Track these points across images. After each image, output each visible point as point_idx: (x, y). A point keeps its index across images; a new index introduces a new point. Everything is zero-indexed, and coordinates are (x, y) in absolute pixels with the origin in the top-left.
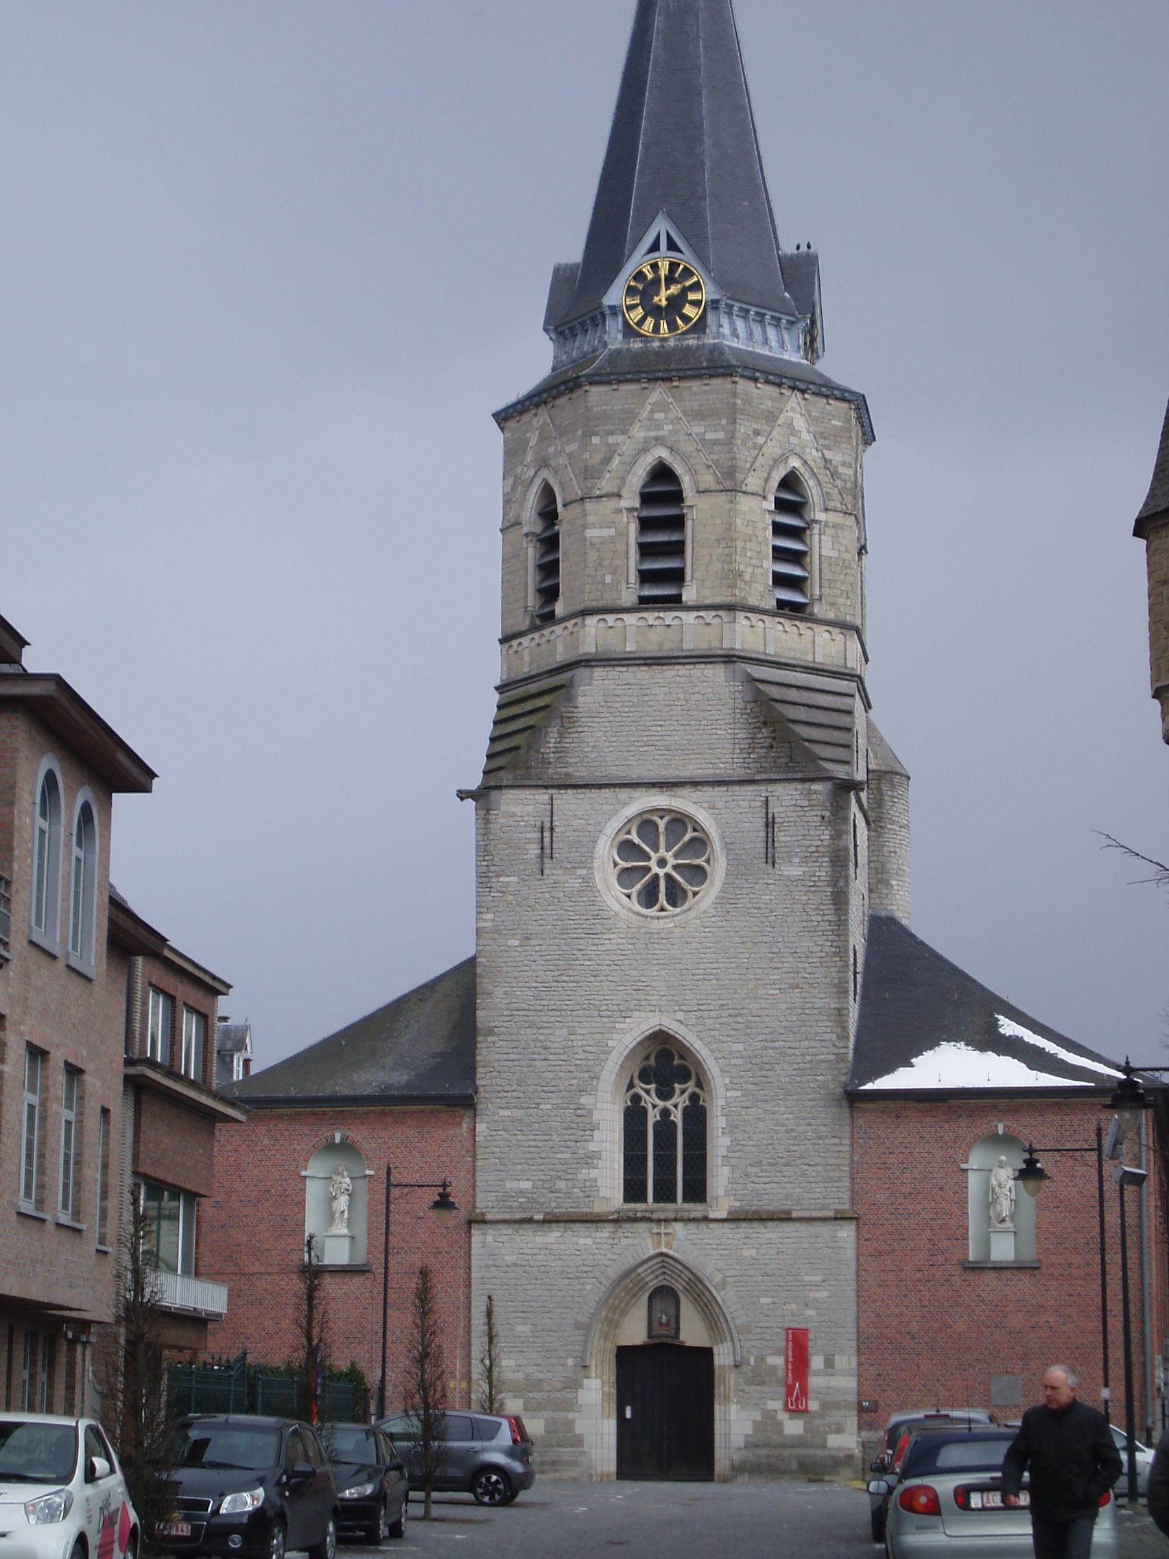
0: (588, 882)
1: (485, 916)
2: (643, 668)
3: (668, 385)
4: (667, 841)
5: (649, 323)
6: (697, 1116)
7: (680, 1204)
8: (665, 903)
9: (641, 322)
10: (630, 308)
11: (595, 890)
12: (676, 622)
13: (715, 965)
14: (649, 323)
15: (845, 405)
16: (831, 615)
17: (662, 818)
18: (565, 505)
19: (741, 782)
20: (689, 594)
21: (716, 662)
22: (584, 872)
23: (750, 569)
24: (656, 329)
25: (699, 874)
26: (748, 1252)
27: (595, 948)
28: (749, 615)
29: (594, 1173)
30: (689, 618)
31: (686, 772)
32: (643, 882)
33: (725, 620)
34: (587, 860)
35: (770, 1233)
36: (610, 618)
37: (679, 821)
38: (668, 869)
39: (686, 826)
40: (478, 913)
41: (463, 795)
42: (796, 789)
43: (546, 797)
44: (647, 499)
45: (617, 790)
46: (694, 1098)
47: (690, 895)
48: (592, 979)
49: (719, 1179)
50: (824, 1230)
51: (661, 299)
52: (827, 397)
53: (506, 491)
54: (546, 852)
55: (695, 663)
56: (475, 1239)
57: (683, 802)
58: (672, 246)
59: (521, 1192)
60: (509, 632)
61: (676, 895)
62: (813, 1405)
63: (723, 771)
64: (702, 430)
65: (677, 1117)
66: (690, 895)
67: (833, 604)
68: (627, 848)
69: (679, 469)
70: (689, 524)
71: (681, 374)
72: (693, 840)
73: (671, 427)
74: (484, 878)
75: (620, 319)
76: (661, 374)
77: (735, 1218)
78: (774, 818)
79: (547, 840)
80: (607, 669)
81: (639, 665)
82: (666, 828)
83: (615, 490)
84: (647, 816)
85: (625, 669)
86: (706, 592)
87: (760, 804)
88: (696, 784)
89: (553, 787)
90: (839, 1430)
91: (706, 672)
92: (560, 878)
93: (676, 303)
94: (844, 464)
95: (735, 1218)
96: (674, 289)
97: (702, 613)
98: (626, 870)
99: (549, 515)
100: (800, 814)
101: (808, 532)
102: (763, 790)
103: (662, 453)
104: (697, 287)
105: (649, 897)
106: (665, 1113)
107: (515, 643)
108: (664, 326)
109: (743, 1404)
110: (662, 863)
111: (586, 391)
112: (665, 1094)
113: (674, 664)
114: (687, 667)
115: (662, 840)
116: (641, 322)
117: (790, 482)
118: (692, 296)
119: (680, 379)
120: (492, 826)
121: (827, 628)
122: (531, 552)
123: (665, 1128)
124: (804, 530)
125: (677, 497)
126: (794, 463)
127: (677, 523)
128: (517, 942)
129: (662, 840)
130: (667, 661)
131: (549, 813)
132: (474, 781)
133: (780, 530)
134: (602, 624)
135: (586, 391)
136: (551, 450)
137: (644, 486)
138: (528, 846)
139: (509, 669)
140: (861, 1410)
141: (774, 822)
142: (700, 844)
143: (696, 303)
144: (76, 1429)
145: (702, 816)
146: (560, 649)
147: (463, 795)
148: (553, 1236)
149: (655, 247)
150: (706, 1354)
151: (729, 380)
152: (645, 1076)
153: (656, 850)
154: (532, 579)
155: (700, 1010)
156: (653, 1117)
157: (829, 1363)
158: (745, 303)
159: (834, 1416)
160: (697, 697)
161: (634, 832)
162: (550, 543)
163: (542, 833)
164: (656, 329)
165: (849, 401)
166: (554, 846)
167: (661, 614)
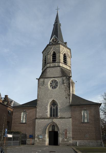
0: (47, 87)
6: (57, 108)
7: (55, 117)
20: (56, 62)
25: (57, 86)
26: (61, 121)
29: (47, 114)
30: (56, 63)
31: (55, 76)
35: (64, 119)
36: (50, 64)
37: (55, 81)
41: (37, 79)
46: (57, 107)
49: (59, 114)
50: (69, 119)
53: (59, 131)
54: (44, 84)
56: (36, 120)
57: (56, 79)
58: (55, 37)
59: (40, 116)
61: (55, 88)
62: (68, 137)
63: (59, 76)
65: (55, 108)
68: (51, 83)
74: (38, 87)
77: (60, 118)
88: (57, 77)
90: (70, 140)
93: (56, 41)
95: (60, 118)
102: (63, 78)
103: (54, 50)
105: (53, 88)
106: (54, 108)
109: (61, 137)
110: (54, 85)
112: (54, 106)
123: (54, 109)
126: (65, 52)
127: (55, 56)
140: (72, 138)
142: (57, 83)
144: (77, 142)
145: (57, 80)
147: (37, 79)
148: (43, 120)
150: (57, 132)
152: (52, 105)
156: (53, 109)
157: (69, 133)
159: (70, 139)
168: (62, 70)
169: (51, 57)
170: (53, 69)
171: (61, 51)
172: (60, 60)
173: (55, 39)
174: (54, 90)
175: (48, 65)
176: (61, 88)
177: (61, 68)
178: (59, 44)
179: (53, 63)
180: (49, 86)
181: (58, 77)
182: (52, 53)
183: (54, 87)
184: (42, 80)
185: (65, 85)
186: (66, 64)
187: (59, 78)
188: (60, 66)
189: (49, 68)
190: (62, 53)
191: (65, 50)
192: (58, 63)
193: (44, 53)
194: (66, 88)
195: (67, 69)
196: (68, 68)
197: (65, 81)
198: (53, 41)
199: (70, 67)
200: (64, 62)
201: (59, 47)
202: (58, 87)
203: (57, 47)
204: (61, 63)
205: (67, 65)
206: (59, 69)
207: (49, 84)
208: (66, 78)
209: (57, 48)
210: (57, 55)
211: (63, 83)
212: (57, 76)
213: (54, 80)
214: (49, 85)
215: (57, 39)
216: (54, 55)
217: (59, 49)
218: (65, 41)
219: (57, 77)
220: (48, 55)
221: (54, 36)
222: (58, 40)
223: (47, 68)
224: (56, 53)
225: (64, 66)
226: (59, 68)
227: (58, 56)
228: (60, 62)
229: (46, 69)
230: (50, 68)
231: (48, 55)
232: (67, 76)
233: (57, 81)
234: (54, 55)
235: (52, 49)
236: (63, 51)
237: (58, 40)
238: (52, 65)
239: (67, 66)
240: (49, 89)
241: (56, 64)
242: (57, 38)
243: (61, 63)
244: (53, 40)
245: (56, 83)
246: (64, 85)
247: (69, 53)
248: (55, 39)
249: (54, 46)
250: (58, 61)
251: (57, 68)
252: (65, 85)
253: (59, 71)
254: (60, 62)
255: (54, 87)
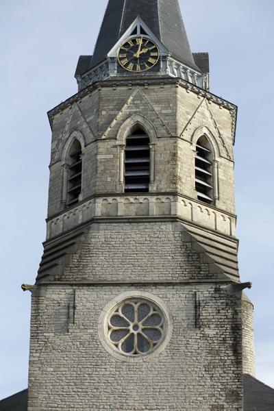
0: (93, 338)
1: (34, 355)
2: (126, 224)
3: (142, 88)
4: (139, 315)
5: (131, 65)
8: (137, 349)
9: (126, 65)
10: (121, 59)
11: (98, 341)
12: (146, 201)
13: (166, 384)
14: (131, 65)
15: (228, 111)
16: (224, 208)
17: (136, 303)
18: (85, 146)
19: (181, 284)
20: (153, 188)
21: (168, 221)
22: (92, 331)
23: (185, 177)
24: (135, 68)
25: (157, 334)
27: (97, 373)
28: (184, 199)
30: (153, 199)
31: (148, 279)
32: (125, 338)
33: (172, 200)
34: (95, 323)
36: (110, 199)
37: (146, 304)
38: (135, 333)
39: (150, 309)
40: (30, 352)
41: (24, 288)
42: (212, 288)
43: (72, 290)
44: (129, 142)
45: (111, 287)
47: (152, 345)
48: (95, 391)
51: (137, 55)
52: (219, 105)
55: (155, 222)
58: (143, 32)
60: (52, 214)
64: (159, 109)
66: (152, 345)
67: (224, 203)
68: (115, 319)
69: (147, 127)
70: (152, 153)
71: (149, 82)
72: (153, 315)
73: (143, 107)
74: (35, 335)
75: (116, 64)
76: (138, 81)
78: (199, 303)
79: (71, 314)
80: (108, 224)
81: (125, 222)
82: (138, 309)
83: (114, 136)
84: (127, 302)
85: (116, 225)
86: (161, 186)
87: (191, 296)
88: (156, 284)
89: (76, 285)
91: (162, 227)
92: (78, 334)
93: (144, 57)
94: (228, 138)
96: (144, 51)
97: (159, 197)
98: (115, 331)
99: (76, 155)
100: (214, 301)
101: (211, 167)
102: (194, 288)
103: (139, 119)
104: (155, 50)
105: (128, 347)
107: (55, 220)
108: (138, 67)
110: (136, 327)
111: (99, 90)
113: (144, 222)
114: (151, 224)
115: (136, 315)
116: (126, 65)
117: (202, 141)
118: (152, 54)
119: (149, 85)
120: (41, 305)
121: (222, 214)
122: (65, 173)
124: (209, 165)
125: (146, 141)
127: (146, 154)
128: (52, 369)
129: (136, 315)
130: (144, 220)
131: (73, 299)
132: (32, 282)
133: (198, 163)
134: (105, 202)
135: (99, 90)
136: (79, 123)
137: (128, 136)
138: (60, 317)
139: (50, 234)
141: (199, 305)
143: (155, 57)
146: (81, 217)
147: (24, 288)
149: (134, 32)
151: (174, 86)
153: (133, 321)
154: (66, 188)
155: (157, 409)
158: (179, 61)
160: (157, 239)
161: (120, 311)
162: (77, 168)
163: (69, 309)
164: (135, 68)
165: (230, 109)
166: (75, 316)
167: (137, 197)
168: (193, 241)
169: (116, 157)
170: (134, 233)
171: (181, 121)
172: (174, 179)
173: (144, 41)
174: (138, 360)
175: (100, 207)
176: (183, 348)
177: (185, 232)
178: (173, 82)
179: (128, 192)
180: (108, 335)
181: (162, 284)
182: (124, 133)
183: (138, 345)
184: (56, 295)
185: (207, 331)
186: (210, 203)
187: (169, 292)
188: (174, 219)
189: (102, 226)
190: (187, 135)
191: (207, 113)
192: (163, 199)
193: (67, 115)
194: (218, 352)
195: (220, 229)
196: (223, 225)
197: (207, 312)
198: (129, 55)
199: (233, 217)
200: (199, 188)
201: (172, 102)
202: (166, 343)
203: (158, 102)
204: (180, 199)
205: (219, 204)
206: (170, 236)
207: (106, 320)
208: (217, 290)
209: (157, 108)
210: (159, 148)
211: (197, 323)
212: (157, 279)
213: (141, 299)
214: (106, 329)
215: (151, 43)
216: (139, 144)
217: (174, 115)
218: (195, 47)
219: (156, 284)
220: (102, 146)
221: (136, 23)
222: (161, 53)
223: (94, 226)
224: (151, 133)
225: (203, 215)
226: (168, 227)
227: (166, 157)
228: (175, 194)
229: (80, 231)
230: (110, 226)
231: (100, 144)
232: (220, 278)
233: (156, 308)
234: (139, 144)
235: (125, 109)
236: (195, 123)
237: (161, 53)
238: (125, 206)
239: (219, 214)
240: (103, 356)
241: (154, 205)
242: (150, 36)
243: (180, 199)
244: (126, 45)
245: (152, 316)
246: (205, 337)
247: (227, 134)
248: (140, 42)
249: (137, 90)
250: (164, 187)
251: (156, 226)
252: (207, 331)
253: (170, 248)
254: (175, 194)
255: (138, 345)
